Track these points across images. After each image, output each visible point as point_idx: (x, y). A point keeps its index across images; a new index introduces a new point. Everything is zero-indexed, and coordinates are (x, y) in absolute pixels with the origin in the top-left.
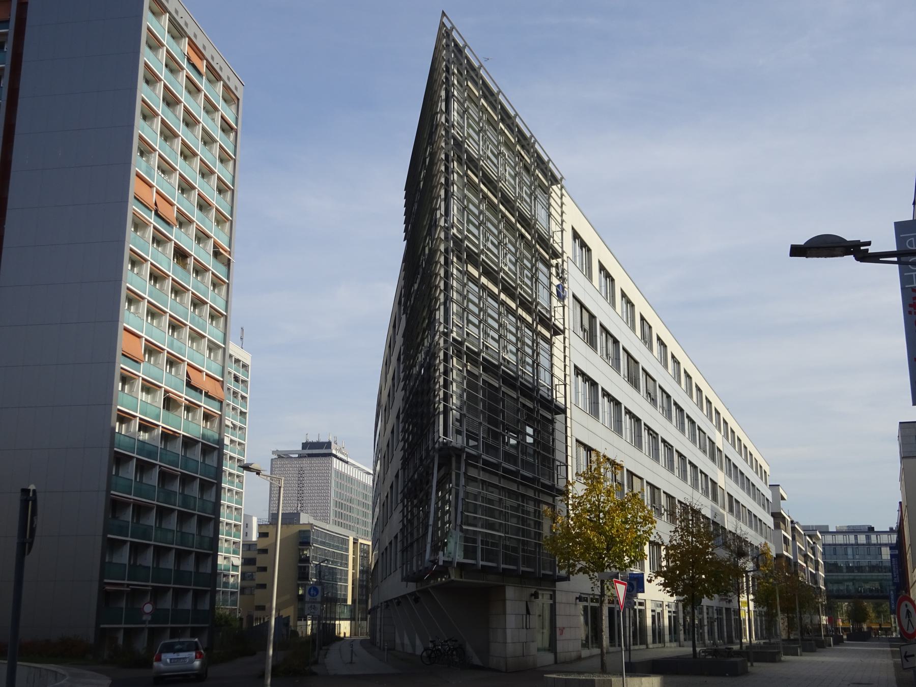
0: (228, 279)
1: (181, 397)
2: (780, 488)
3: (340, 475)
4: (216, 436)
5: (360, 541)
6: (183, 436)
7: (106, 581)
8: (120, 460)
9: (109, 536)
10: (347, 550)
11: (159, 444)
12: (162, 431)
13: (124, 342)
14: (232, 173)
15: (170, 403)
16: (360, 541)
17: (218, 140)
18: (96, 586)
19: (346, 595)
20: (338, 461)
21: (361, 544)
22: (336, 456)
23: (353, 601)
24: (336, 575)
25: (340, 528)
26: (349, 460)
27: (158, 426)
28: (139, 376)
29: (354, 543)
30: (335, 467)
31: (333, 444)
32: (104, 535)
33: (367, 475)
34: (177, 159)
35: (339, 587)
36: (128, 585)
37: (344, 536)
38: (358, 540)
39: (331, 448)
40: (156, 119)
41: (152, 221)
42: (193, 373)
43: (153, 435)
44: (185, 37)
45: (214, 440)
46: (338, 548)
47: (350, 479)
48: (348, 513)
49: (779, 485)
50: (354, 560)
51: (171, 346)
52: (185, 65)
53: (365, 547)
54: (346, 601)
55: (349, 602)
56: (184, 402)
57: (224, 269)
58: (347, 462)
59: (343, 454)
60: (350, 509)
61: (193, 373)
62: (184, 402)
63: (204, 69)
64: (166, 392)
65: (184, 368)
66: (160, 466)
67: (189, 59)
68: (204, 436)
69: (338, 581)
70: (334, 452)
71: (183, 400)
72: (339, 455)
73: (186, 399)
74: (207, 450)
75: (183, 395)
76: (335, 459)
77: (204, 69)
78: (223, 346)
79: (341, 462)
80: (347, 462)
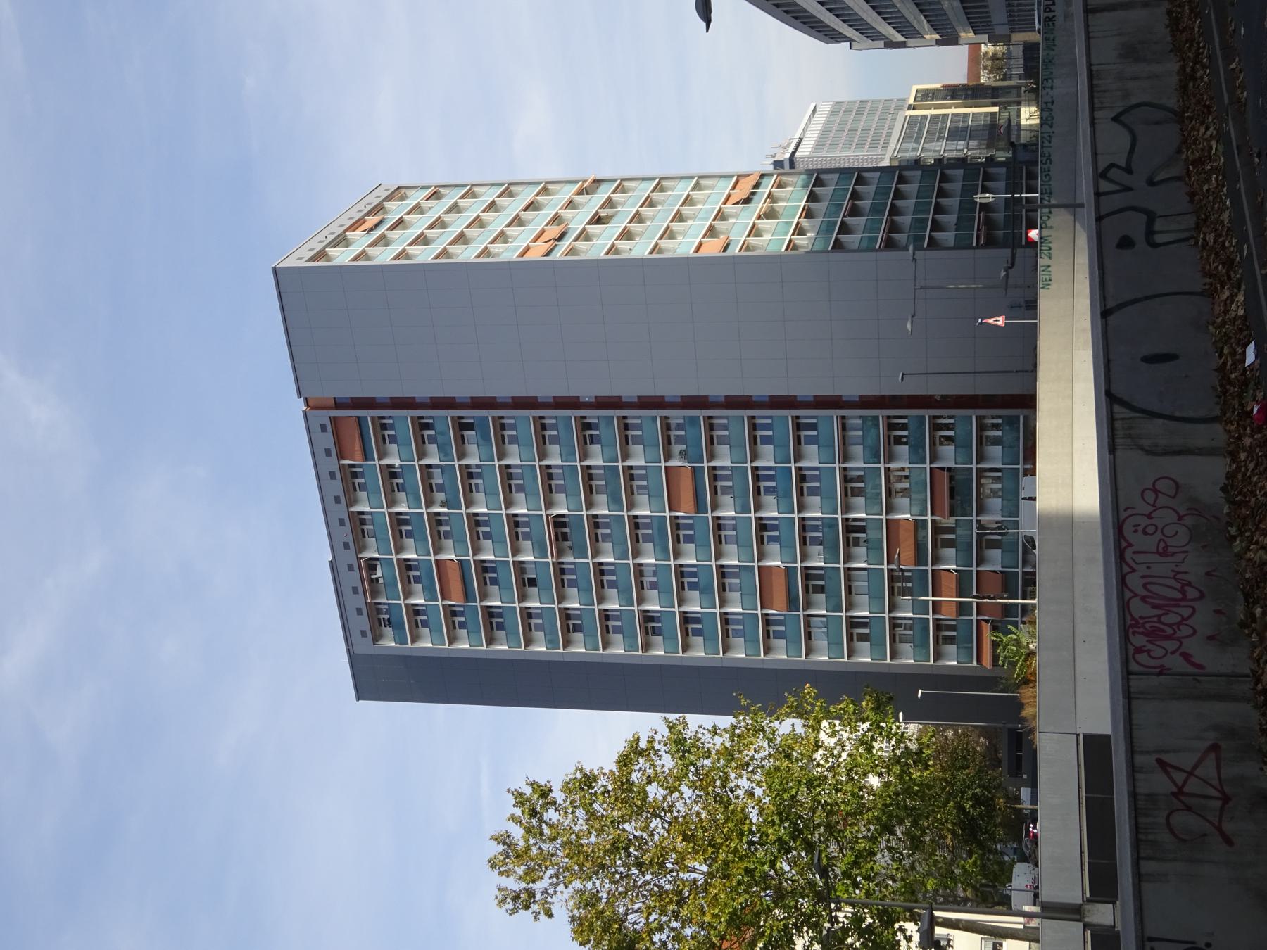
0: (615, 180)
1: (762, 207)
2: (280, 265)
3: (819, 145)
4: (804, 177)
5: (911, 101)
6: (807, 201)
7: (974, 244)
8: (838, 245)
9: (925, 246)
10: (925, 117)
11: (818, 221)
12: (805, 218)
13: (712, 248)
14: (488, 188)
15: (770, 214)
16: (911, 101)
17: (454, 201)
18: (980, 252)
19: (986, 114)
20: (799, 150)
21: (915, 100)
22: (794, 153)
23: (994, 105)
24: (958, 127)
25: (894, 131)
26: (797, 136)
27: (798, 223)
28: (745, 240)
29: (914, 109)
30: (808, 153)
31: (776, 159)
32: (925, 249)
33: (817, 113)
34: (490, 231)
35: (975, 124)
36: (979, 229)
37: (905, 121)
38: (910, 105)
39: (782, 161)
40: (450, 251)
41: (568, 243)
42: (732, 200)
43: (809, 228)
44: (346, 236)
45: (808, 178)
46: (921, 129)
47: (824, 133)
48: (871, 133)
49: (274, 269)
50: (937, 107)
51: (707, 219)
52: (377, 233)
53: (919, 95)
54: (993, 114)
55: (996, 109)
56: (768, 204)
57: (603, 187)
58: (801, 140)
59: (789, 145)
60: (866, 130)
61: (732, 200)
62: (768, 204)
63: (376, 219)
64: (759, 218)
65: (729, 208)
66: (844, 216)
67: (372, 229)
68: (805, 186)
69: (966, 124)
70: (787, 156)
71: (765, 205)
72: (791, 149)
73: (764, 203)
74: (819, 183)
75: (760, 206)
76: (797, 154)
77: (376, 219)
78: (696, 179)
79: (801, 146)
80: (801, 140)
